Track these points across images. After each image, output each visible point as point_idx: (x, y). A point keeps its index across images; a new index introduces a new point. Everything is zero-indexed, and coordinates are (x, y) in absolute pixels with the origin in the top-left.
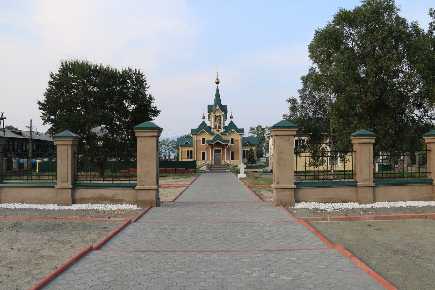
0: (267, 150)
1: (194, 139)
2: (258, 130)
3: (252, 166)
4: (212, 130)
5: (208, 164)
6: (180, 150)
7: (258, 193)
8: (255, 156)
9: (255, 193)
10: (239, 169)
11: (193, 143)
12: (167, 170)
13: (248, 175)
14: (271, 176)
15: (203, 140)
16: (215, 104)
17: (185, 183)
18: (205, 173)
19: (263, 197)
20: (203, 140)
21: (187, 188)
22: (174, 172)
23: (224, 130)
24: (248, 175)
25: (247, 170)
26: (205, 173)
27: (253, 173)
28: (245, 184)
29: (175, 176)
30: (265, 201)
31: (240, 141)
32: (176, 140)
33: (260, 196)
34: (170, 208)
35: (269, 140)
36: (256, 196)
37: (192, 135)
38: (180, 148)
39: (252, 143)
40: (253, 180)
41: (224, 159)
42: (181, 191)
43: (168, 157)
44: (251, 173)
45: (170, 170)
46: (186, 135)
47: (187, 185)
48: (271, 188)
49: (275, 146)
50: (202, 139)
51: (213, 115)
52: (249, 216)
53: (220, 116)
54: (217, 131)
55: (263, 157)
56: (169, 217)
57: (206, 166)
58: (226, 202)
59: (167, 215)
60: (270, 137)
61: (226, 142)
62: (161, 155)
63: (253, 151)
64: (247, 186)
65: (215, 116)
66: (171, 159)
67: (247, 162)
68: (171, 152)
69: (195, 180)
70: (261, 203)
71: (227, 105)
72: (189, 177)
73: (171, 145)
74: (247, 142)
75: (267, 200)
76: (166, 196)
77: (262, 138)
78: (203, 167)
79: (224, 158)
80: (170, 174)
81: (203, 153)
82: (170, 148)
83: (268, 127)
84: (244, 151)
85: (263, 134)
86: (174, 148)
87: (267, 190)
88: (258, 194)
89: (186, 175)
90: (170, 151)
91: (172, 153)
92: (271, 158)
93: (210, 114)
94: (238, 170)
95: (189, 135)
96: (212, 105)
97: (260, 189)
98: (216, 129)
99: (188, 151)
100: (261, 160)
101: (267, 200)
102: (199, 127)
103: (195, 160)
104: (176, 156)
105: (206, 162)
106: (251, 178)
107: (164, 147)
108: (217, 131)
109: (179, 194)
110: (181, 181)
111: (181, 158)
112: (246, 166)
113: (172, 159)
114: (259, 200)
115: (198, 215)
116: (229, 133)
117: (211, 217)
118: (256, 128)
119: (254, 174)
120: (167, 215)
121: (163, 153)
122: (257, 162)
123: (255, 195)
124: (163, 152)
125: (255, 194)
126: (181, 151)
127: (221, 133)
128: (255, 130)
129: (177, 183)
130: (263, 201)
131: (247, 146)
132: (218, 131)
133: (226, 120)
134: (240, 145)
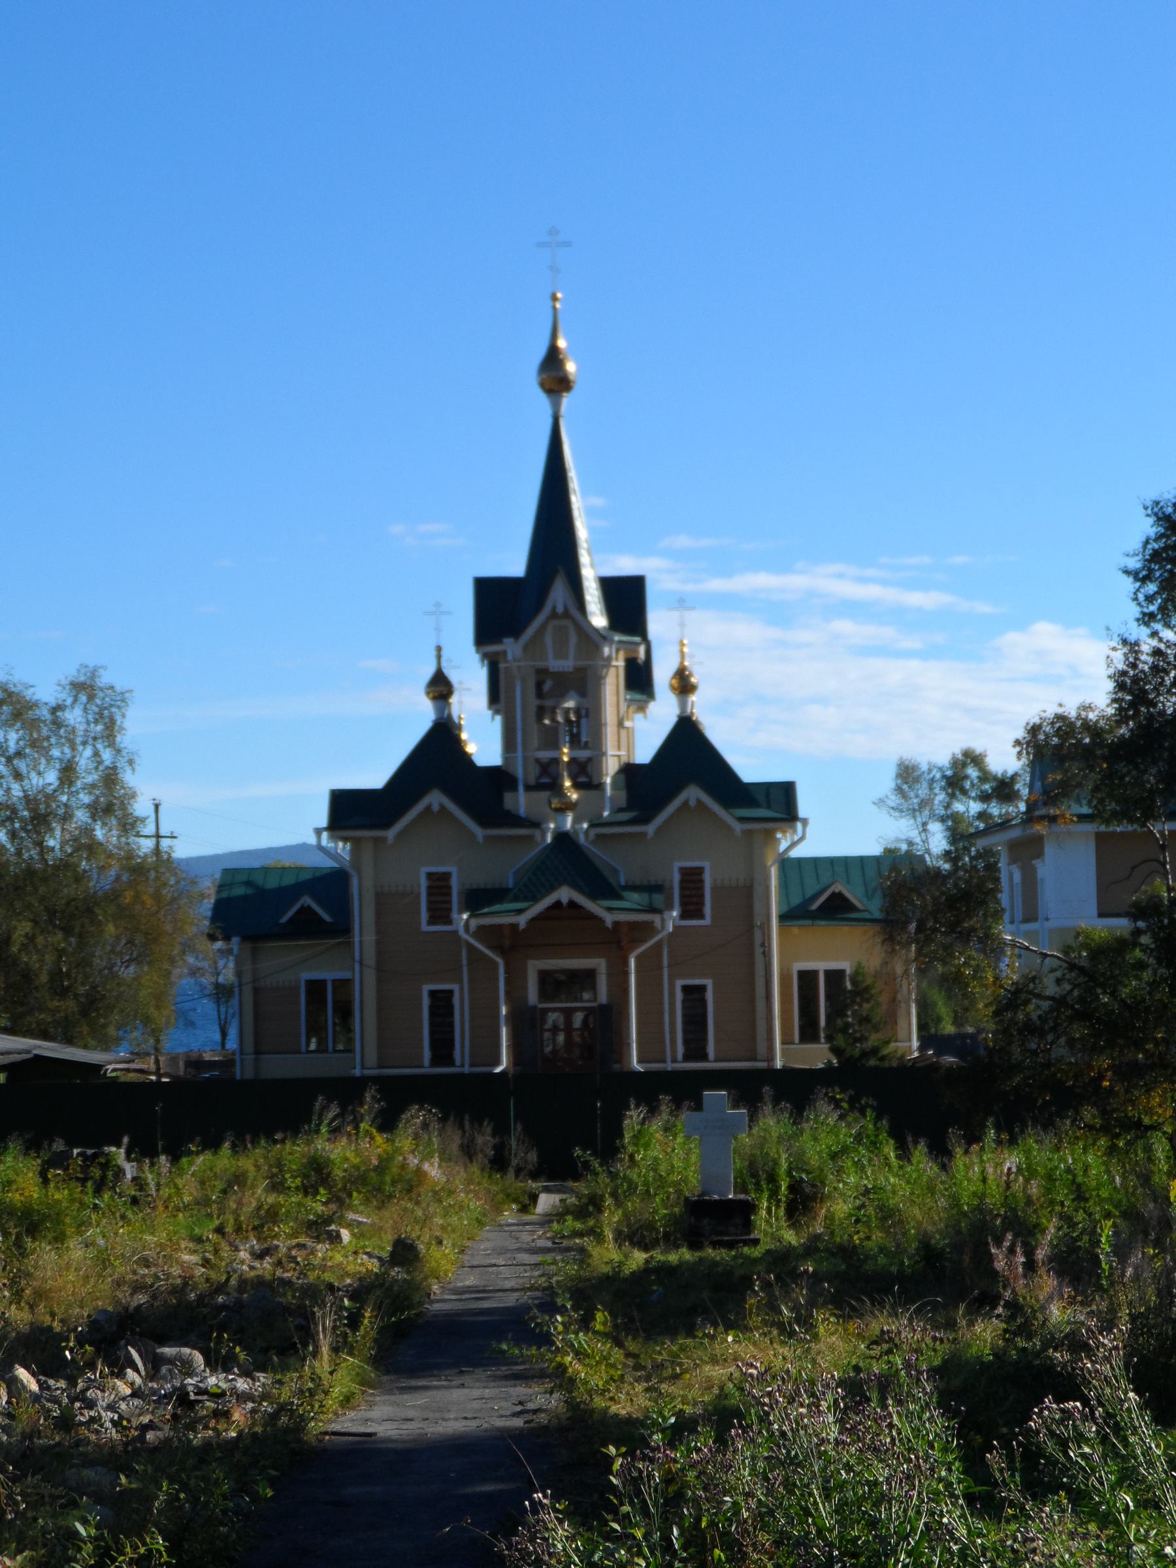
65: (542, 674)
84: (807, 979)
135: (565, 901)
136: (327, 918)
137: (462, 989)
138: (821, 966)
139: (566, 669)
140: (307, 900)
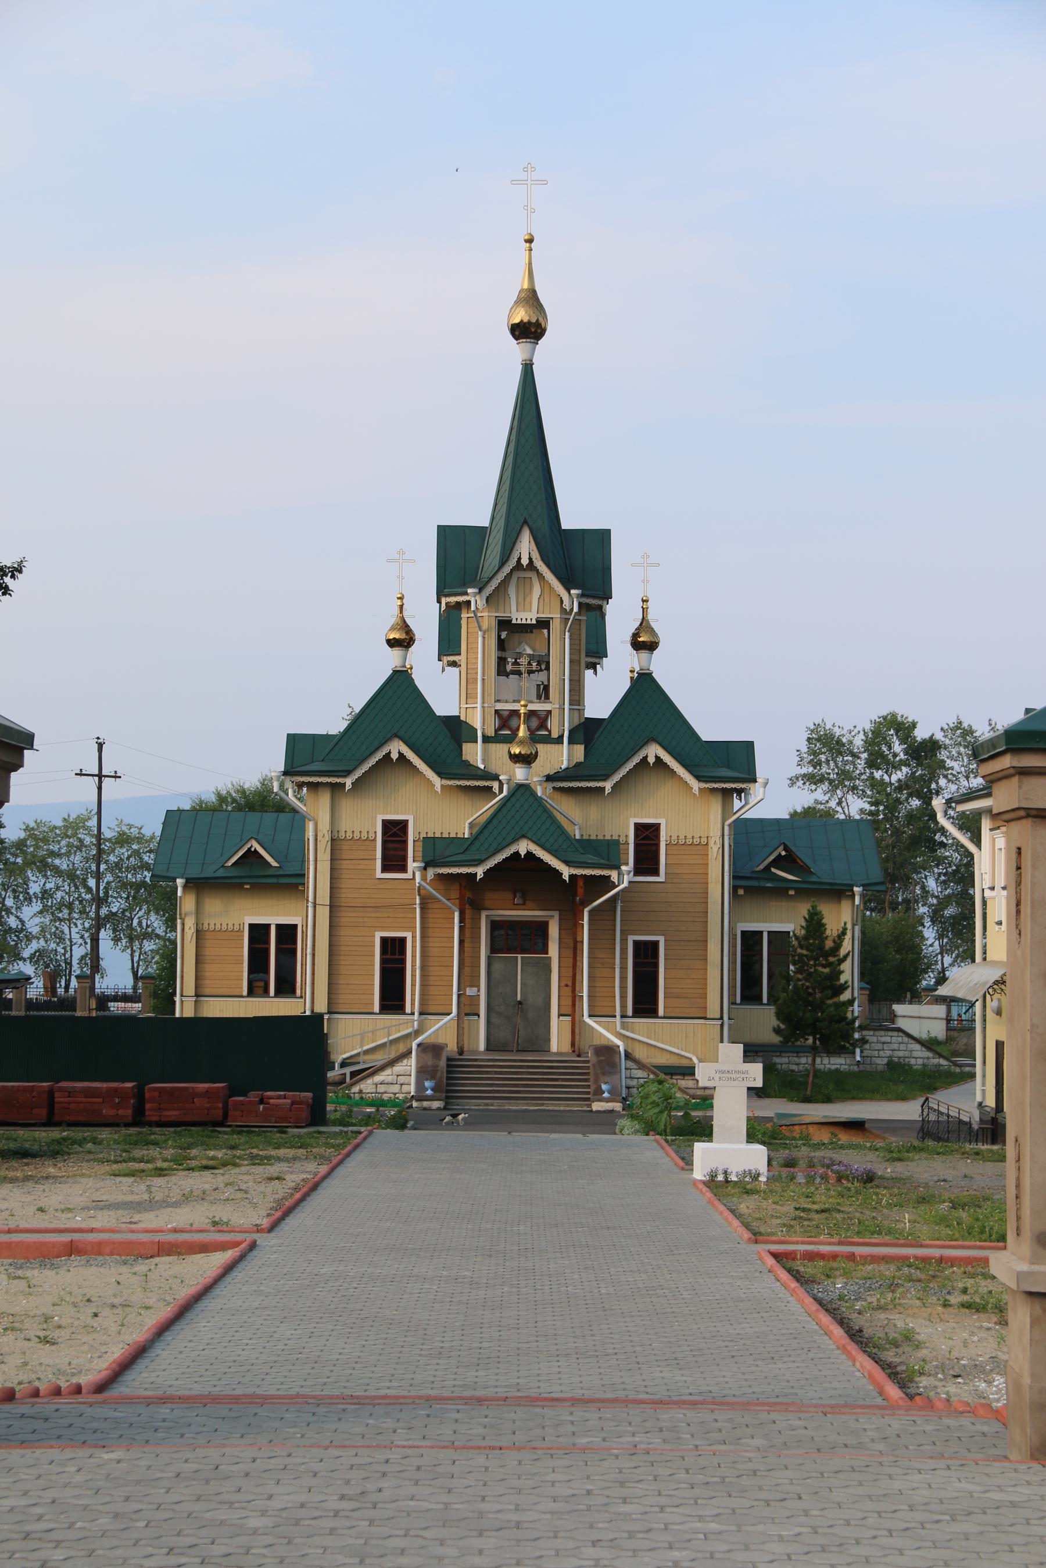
0: (958, 934)
1: (310, 827)
2: (883, 757)
3: (818, 1074)
4: (475, 753)
5: (432, 1049)
6: (190, 923)
7: (872, 1324)
8: (843, 988)
9: (842, 1322)
10: (706, 1100)
11: (303, 860)
12: (58, 1097)
13: (783, 1154)
14: (990, 1167)
15: (395, 831)
16: (501, 523)
17: (222, 1213)
18: (400, 1123)
19: (913, 1359)
20: (395, 831)
21: (242, 1257)
22: (128, 1113)
23: (579, 751)
24: (783, 1154)
25: (772, 1108)
26: (402, 1127)
27: (824, 1136)
28: (757, 1237)
29: (138, 1153)
30: (929, 1405)
31: (714, 849)
32: (153, 827)
33: (890, 1356)
34: (68, 1453)
35: (972, 848)
36: (852, 1347)
37: (300, 785)
38: (187, 903)
39: (823, 871)
40: (823, 1198)
41: (571, 1010)
42: (185, 1293)
43: (74, 983)
44: (806, 1139)
45: (89, 1093)
46: (243, 792)
47: (239, 1237)
48: (985, 1286)
49: (1026, 909)
50: (387, 825)
51: (488, 618)
52: (781, 1539)
53: (543, 624)
54: (516, 758)
55: (916, 997)
56: (58, 1544)
57: (411, 1065)
58: (575, 1401)
59: (40, 1518)
60: (986, 824)
61: (590, 858)
62: (18, 957)
63: (829, 944)
64: (776, 1256)
65: (504, 624)
66: (103, 1001)
67: (776, 1039)
68: (105, 935)
69: (315, 1187)
70: (896, 1423)
71: (604, 536)
72: (256, 1160)
73: (109, 877)
74: (778, 862)
75: (952, 1389)
76: (45, 1341)
77: (909, 831)
78: (382, 1068)
79: (575, 998)
80: (87, 1133)
81: (394, 949)
82: (100, 901)
83: (969, 732)
84: (751, 940)
85: (919, 795)
86: (135, 901)
87: (955, 1299)
88: (868, 1332)
89: (235, 1139)
90: (99, 923)
91: (116, 940)
92: (992, 1004)
93: (458, 606)
94: (696, 1107)
95: (266, 784)
96: (480, 533)
97: (892, 1287)
98: (510, 739)
99: (259, 932)
100: (901, 1023)
101: (952, 1389)
102: (358, 721)
103: (321, 1007)
104: (153, 969)
105: (417, 1033)
106: (810, 1180)
107: (45, 894)
108: (516, 758)
109: (164, 1312)
110: (187, 1198)
111: (190, 989)
112: (768, 1071)
113: (116, 998)
114: (881, 1392)
115: (328, 1523)
116: (617, 777)
117: (442, 1543)
118: (859, 742)
119: (835, 1146)
120: (40, 1518)
121: (34, 946)
122: (863, 1041)
123: (845, 1340)
124: (29, 938)
125: (838, 1331)
126: (198, 932)
127: (549, 778)
128: (855, 756)
129: (150, 1220)
130: (911, 1397)
131: (780, 891)
132: (527, 760)
133: (593, 666)
134: (714, 891)
135: (523, 853)
136: (274, 864)
137: (414, 937)
138: (765, 927)
139: (529, 622)
140: (661, 878)
